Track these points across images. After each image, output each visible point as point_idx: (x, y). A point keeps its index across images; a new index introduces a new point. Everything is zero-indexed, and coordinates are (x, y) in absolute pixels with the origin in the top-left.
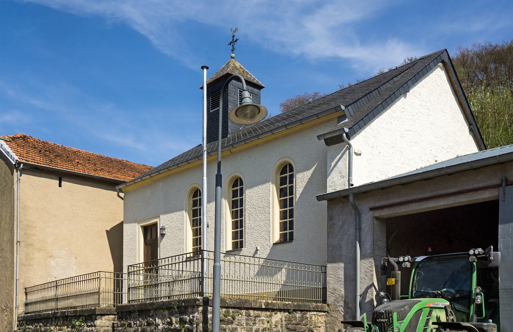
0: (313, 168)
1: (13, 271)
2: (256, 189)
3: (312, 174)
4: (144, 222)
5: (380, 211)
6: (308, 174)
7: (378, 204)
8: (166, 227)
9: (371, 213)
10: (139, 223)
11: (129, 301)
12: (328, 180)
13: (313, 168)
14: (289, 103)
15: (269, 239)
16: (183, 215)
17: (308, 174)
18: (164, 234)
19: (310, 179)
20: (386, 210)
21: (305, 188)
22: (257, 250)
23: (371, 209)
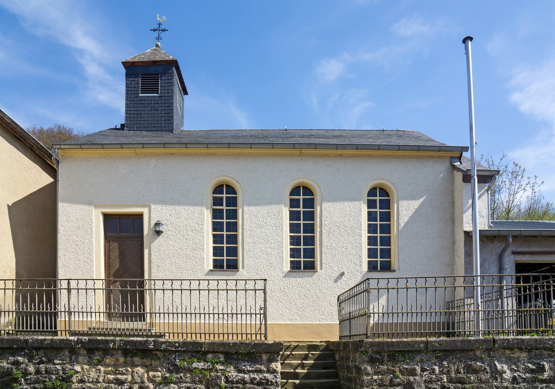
0: (422, 200)
1: (91, 250)
2: (338, 205)
3: (420, 205)
4: (120, 208)
5: (521, 256)
6: (415, 204)
7: (519, 250)
8: (163, 222)
9: (512, 256)
10: (97, 206)
11: (341, 337)
12: (464, 216)
13: (422, 200)
14: (56, 130)
15: (361, 265)
16: (202, 214)
17: (415, 204)
18: (162, 232)
19: (417, 211)
20: (527, 256)
21: (412, 218)
22: (344, 273)
23: (514, 253)
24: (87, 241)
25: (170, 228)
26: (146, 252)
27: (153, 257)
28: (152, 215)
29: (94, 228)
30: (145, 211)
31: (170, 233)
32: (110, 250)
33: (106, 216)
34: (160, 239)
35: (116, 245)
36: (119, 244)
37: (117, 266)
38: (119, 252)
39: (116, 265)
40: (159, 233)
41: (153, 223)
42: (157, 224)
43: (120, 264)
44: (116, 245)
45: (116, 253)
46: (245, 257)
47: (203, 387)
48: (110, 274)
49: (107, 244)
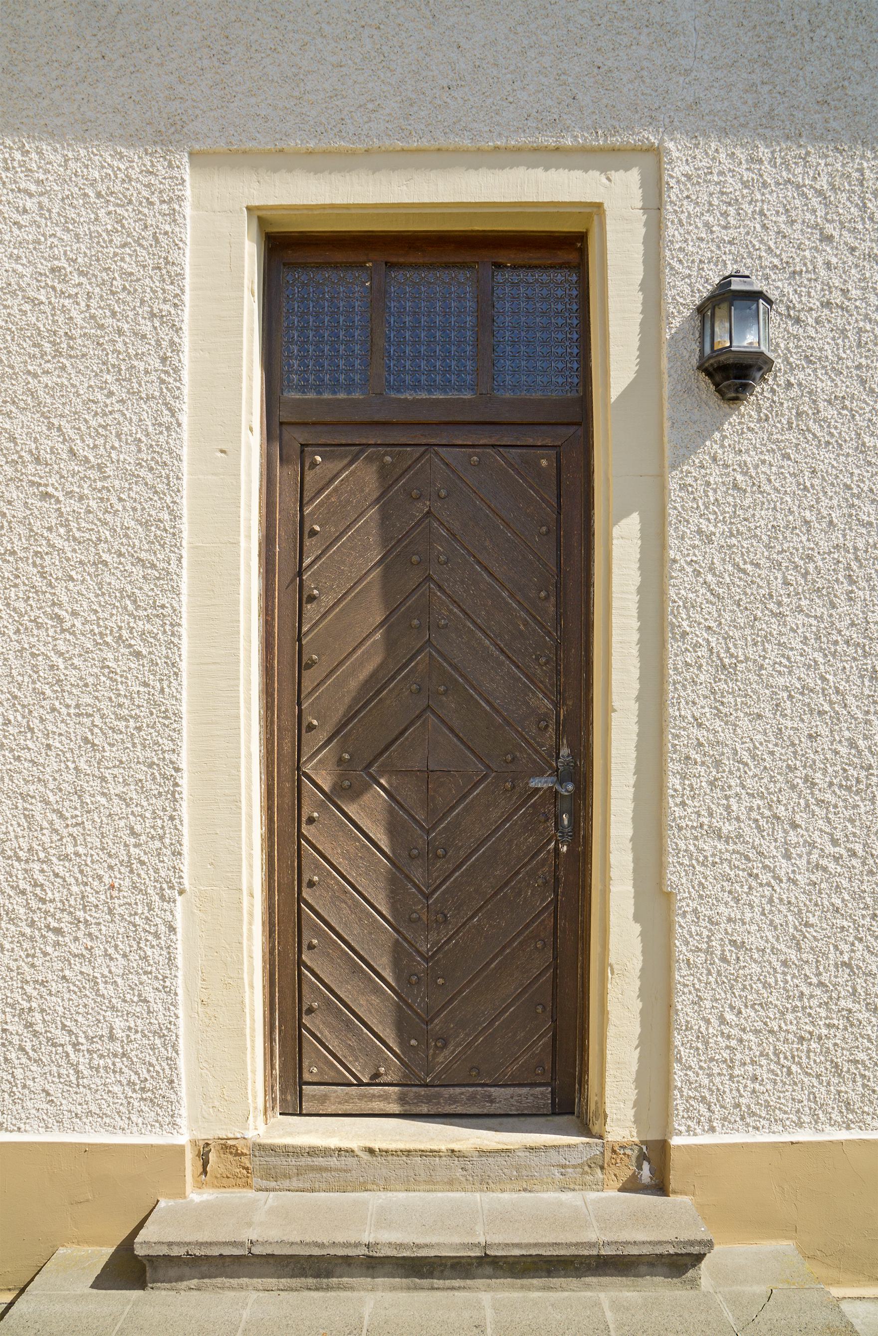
1: (164, 535)
24: (128, 457)
25: (824, 341)
26: (621, 546)
27: (681, 586)
28: (665, 225)
29: (186, 341)
30: (617, 194)
31: (823, 385)
32: (303, 532)
33: (289, 250)
34: (744, 429)
35: (358, 481)
36: (383, 473)
37: (368, 661)
38: (385, 539)
39: (355, 643)
40: (733, 376)
41: (686, 292)
42: (732, 298)
43: (390, 644)
44: (358, 481)
45: (354, 558)
46: (686, 706)
47: (310, 719)
48: (302, 727)
49: (286, 475)
